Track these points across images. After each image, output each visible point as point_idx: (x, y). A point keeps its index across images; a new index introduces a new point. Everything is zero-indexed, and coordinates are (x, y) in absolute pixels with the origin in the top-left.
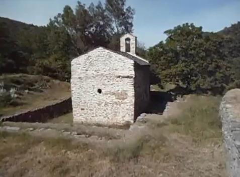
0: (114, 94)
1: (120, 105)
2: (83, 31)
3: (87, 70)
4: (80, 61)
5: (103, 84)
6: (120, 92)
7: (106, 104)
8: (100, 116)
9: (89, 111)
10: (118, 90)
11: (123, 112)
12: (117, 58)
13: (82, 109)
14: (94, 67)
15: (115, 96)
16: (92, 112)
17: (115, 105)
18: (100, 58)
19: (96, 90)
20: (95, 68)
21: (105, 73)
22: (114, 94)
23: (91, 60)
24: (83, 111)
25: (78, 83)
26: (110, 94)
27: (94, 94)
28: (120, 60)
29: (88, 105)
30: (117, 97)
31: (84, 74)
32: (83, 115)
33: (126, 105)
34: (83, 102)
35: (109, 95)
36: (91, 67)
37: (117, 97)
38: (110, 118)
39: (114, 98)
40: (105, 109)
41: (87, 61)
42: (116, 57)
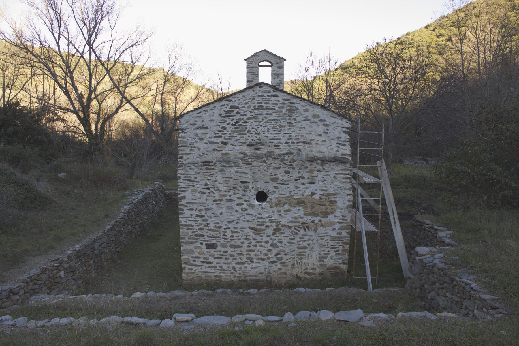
0: (300, 203)
1: (315, 230)
2: (402, 90)
3: (225, 144)
4: (207, 119)
5: (273, 180)
6: (317, 197)
7: (277, 230)
8: (263, 260)
9: (229, 250)
10: (313, 194)
11: (322, 245)
12: (309, 114)
13: (210, 246)
14: (245, 137)
15: (305, 208)
16: (238, 250)
17: (302, 232)
18: (265, 112)
19: (251, 195)
20: (248, 138)
21: (277, 152)
22: (300, 203)
23: (238, 116)
24: (212, 251)
25: (199, 178)
26: (290, 204)
27: (245, 206)
28: (316, 120)
29: (229, 233)
30: (309, 210)
31: (219, 154)
32: (211, 259)
33: (329, 229)
34: (211, 226)
35: (287, 207)
36: (294, 270)
37: (309, 210)
38: (289, 264)
39: (302, 213)
40: (276, 242)
41: (228, 120)
42: (306, 110)
